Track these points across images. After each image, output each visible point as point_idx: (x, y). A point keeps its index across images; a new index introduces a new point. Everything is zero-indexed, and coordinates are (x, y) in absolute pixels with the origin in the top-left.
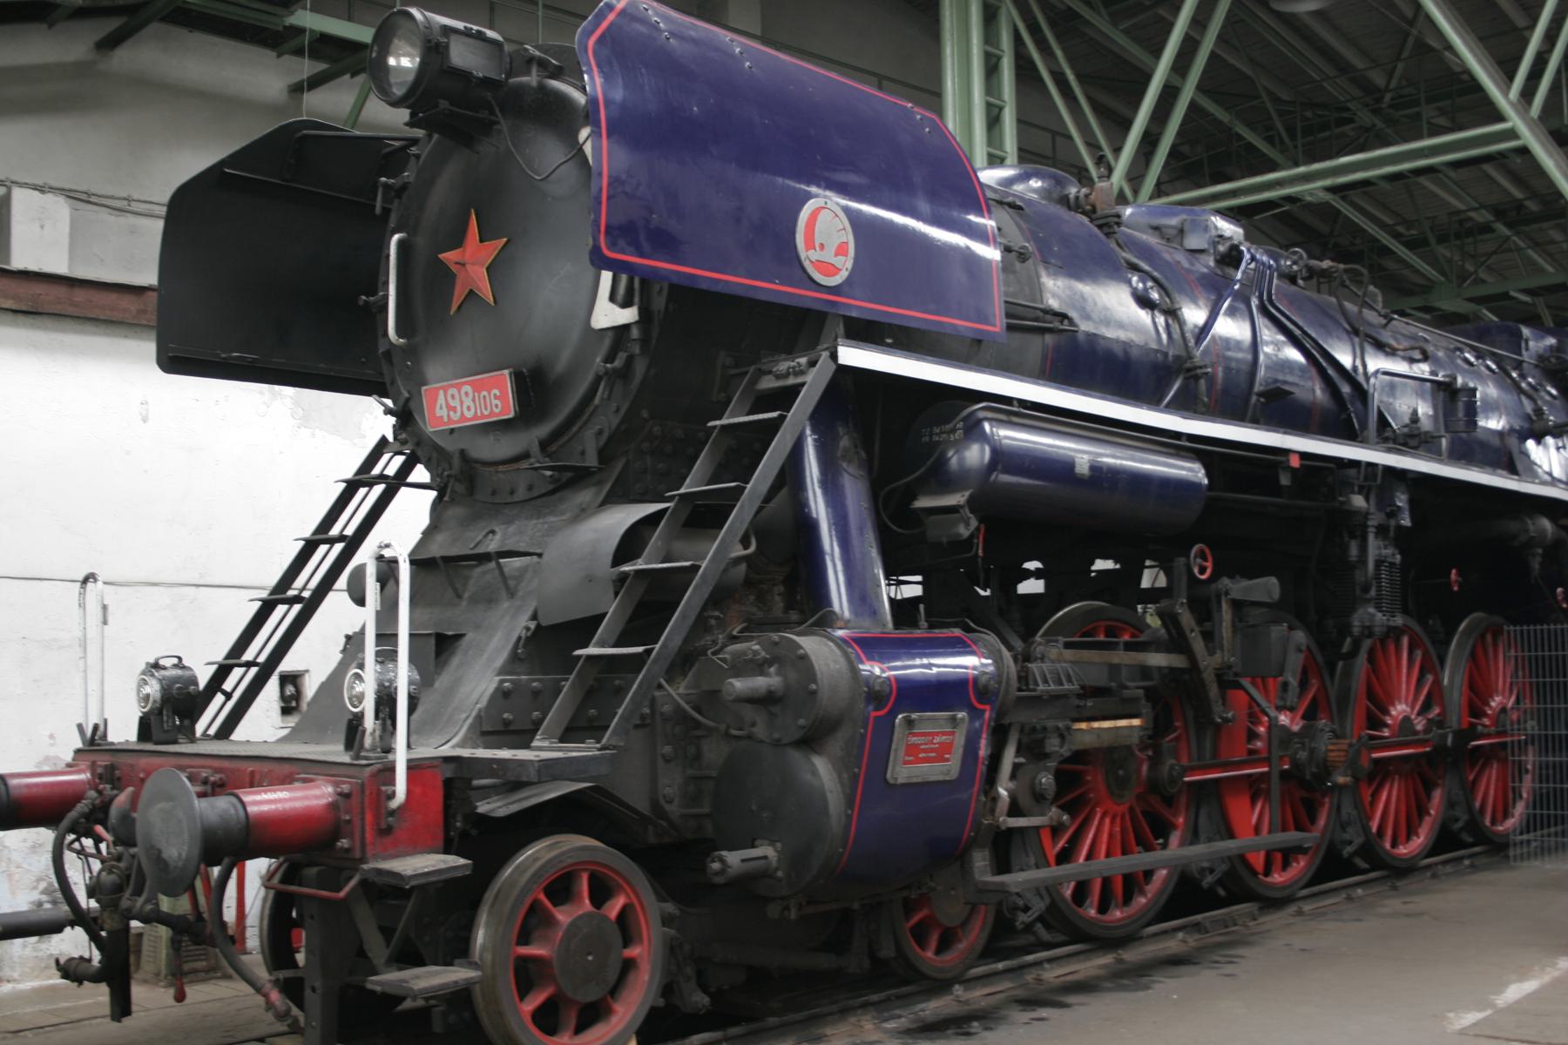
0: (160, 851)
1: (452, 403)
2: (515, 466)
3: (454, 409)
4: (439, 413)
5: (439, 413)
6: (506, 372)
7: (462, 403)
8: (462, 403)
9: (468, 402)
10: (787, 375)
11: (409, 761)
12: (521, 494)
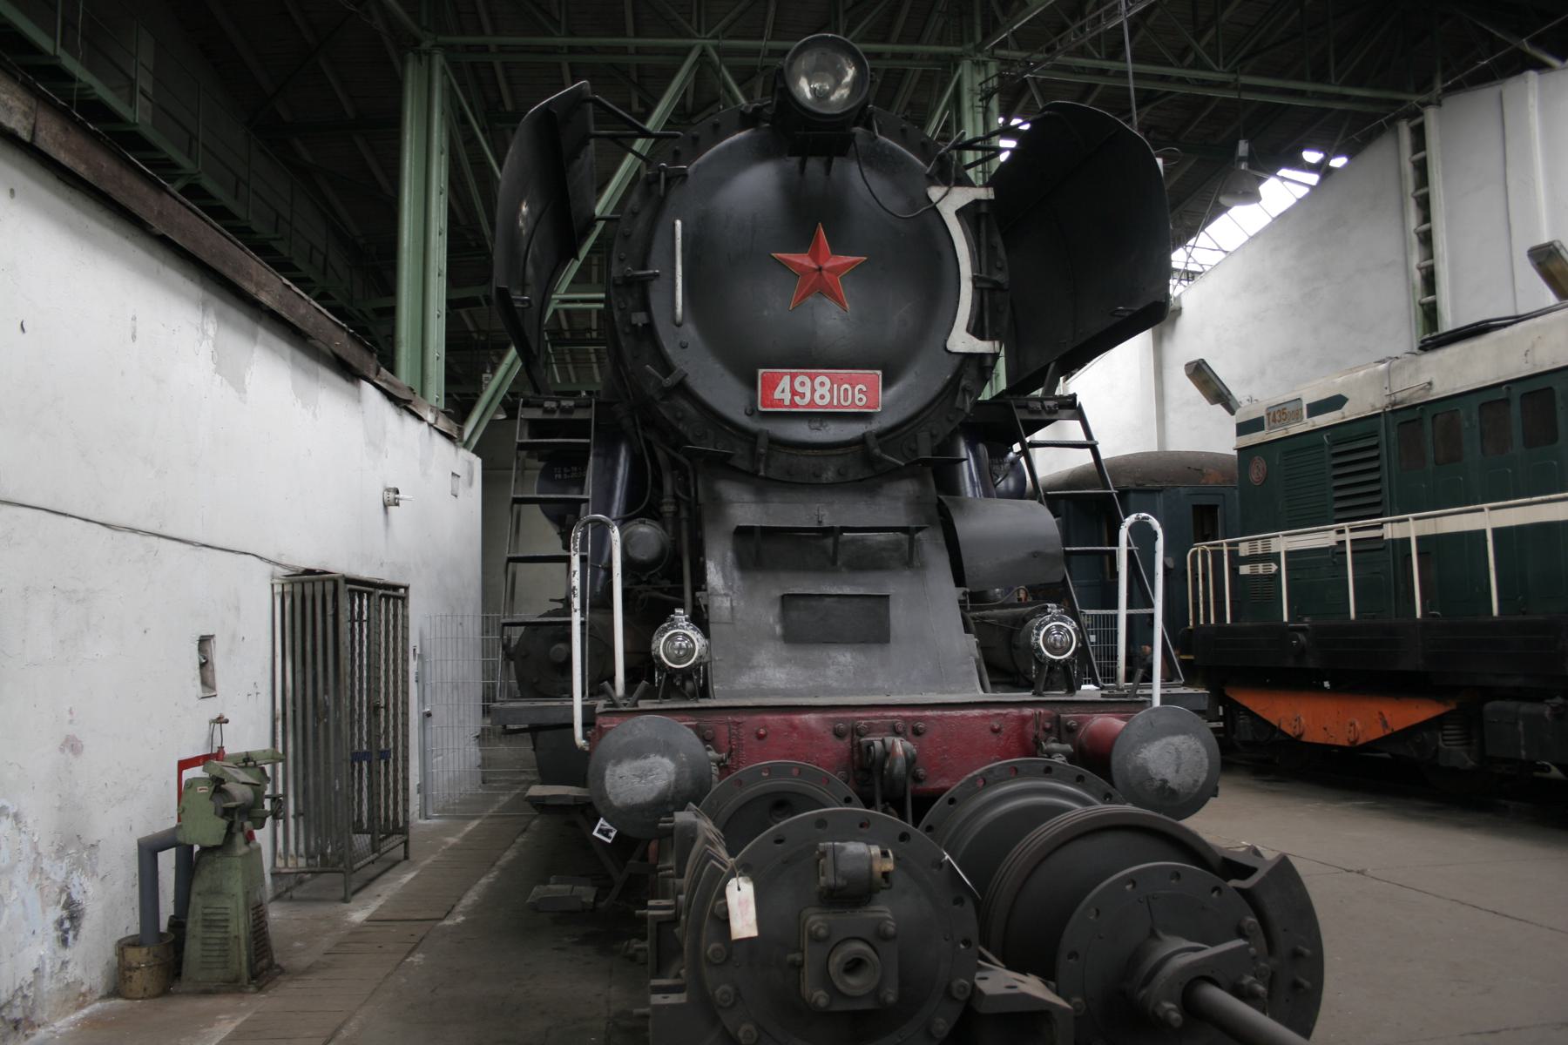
0: (1165, 781)
1: (799, 389)
2: (819, 452)
3: (803, 396)
4: (777, 395)
5: (777, 395)
6: (761, 371)
7: (813, 391)
8: (813, 391)
9: (825, 391)
10: (1038, 412)
11: (1162, 696)
12: (829, 475)
